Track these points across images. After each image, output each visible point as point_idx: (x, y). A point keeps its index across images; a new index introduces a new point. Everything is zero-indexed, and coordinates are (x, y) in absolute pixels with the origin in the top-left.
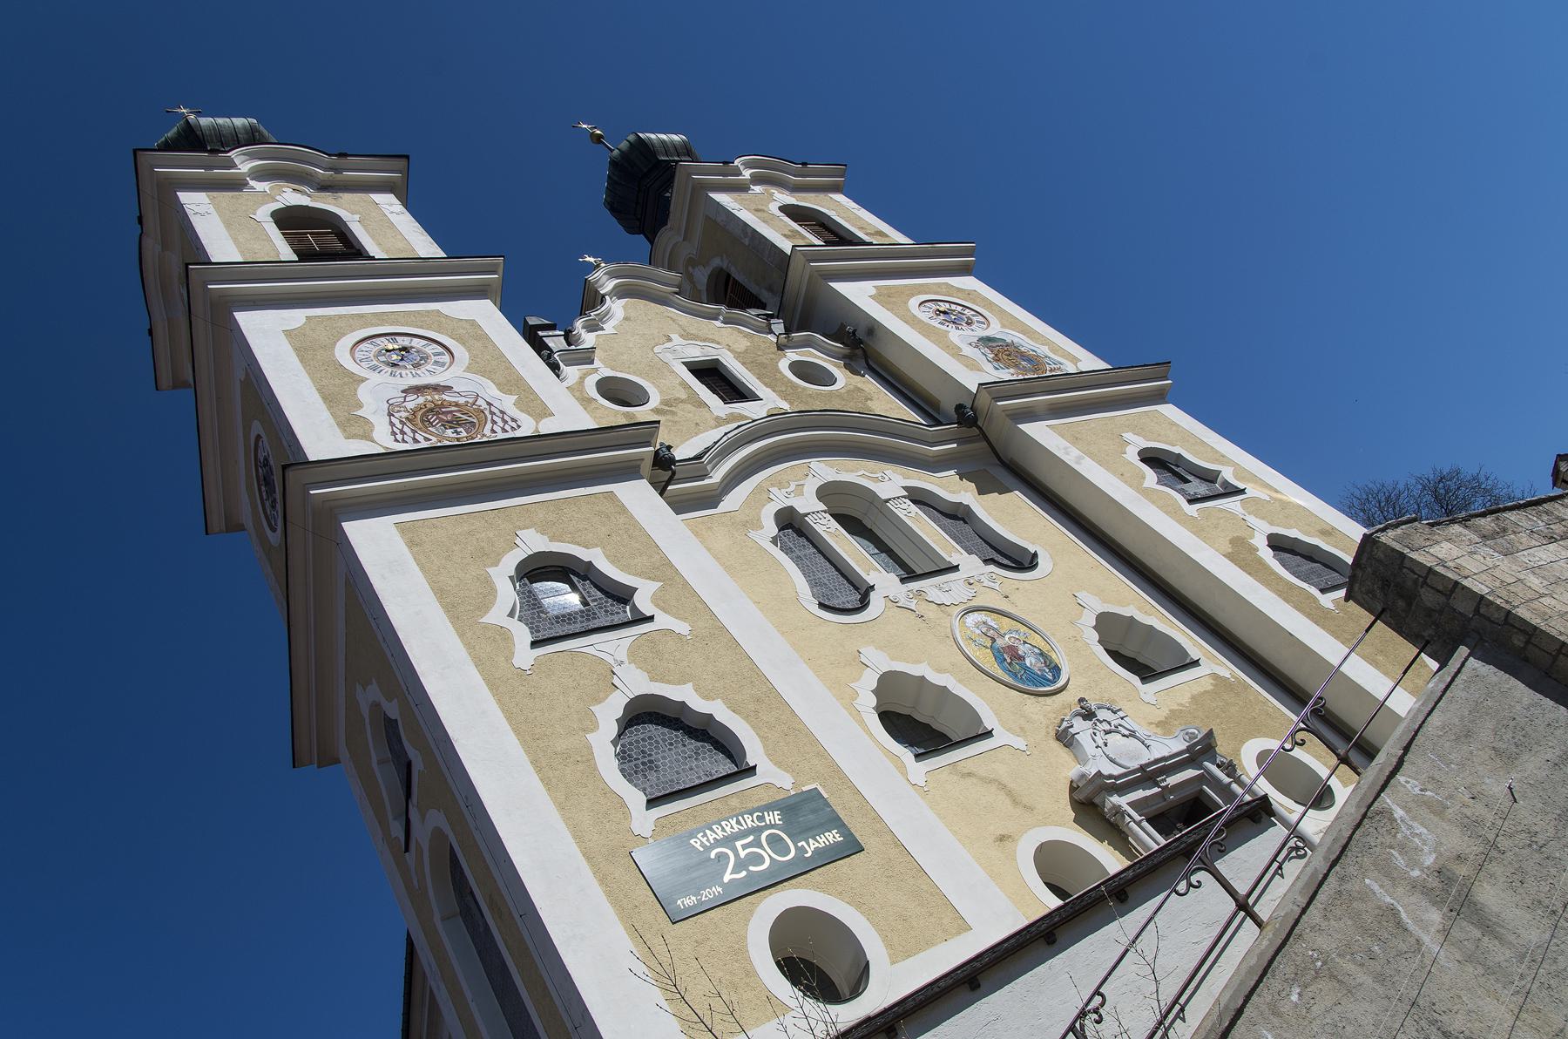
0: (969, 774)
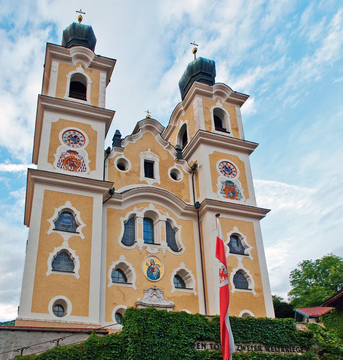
0: (120, 290)
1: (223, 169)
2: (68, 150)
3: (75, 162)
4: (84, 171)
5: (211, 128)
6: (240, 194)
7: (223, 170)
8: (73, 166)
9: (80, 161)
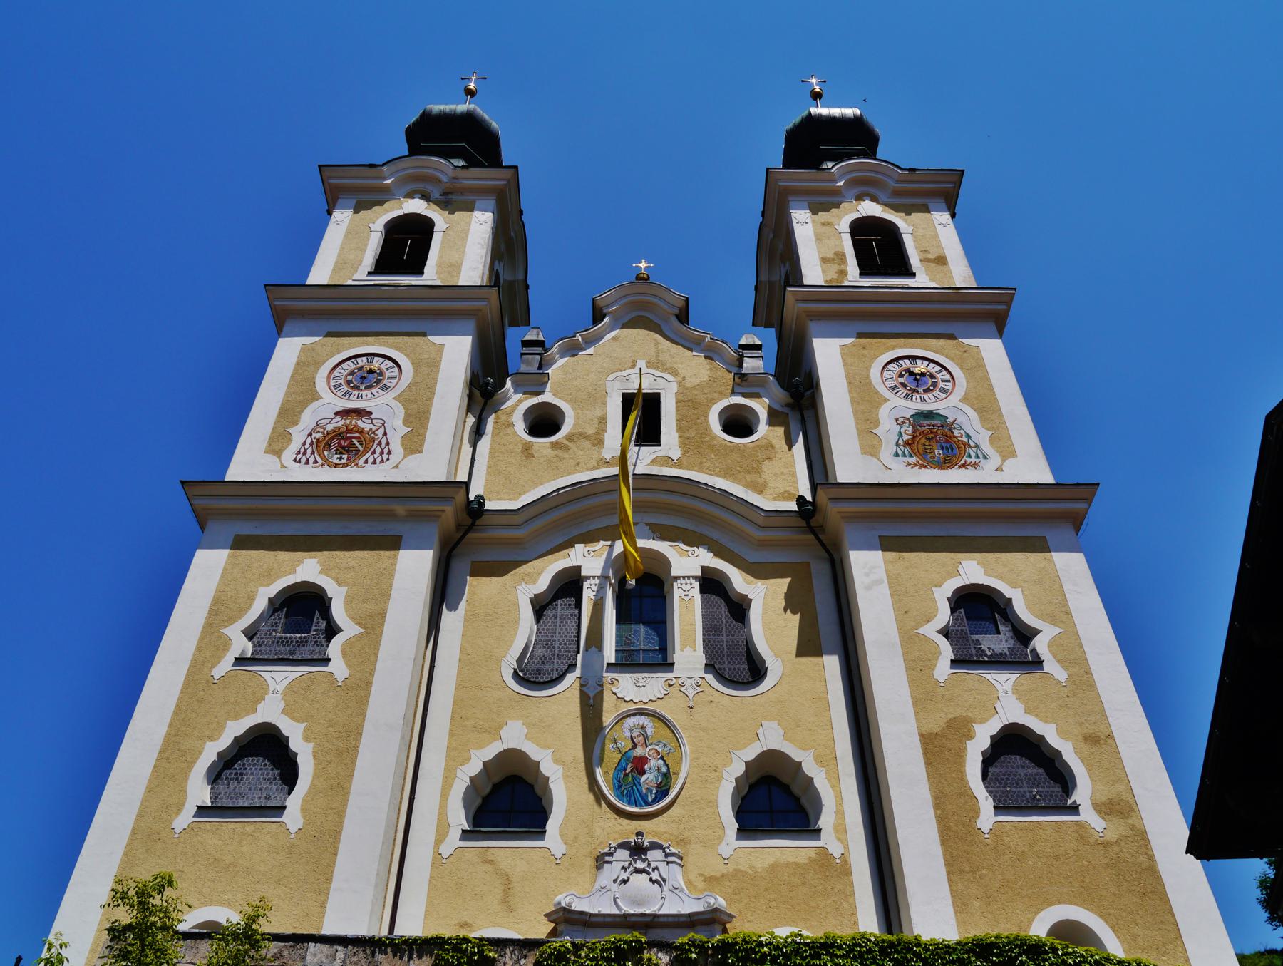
0: (490, 862)
1: (901, 380)
2: (341, 409)
3: (355, 441)
4: (382, 461)
5: (843, 273)
6: (977, 446)
7: (901, 383)
8: (348, 451)
9: (373, 435)
